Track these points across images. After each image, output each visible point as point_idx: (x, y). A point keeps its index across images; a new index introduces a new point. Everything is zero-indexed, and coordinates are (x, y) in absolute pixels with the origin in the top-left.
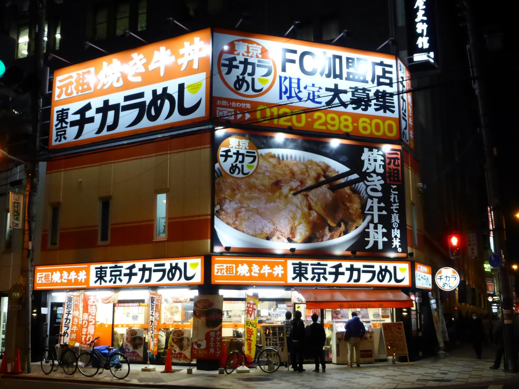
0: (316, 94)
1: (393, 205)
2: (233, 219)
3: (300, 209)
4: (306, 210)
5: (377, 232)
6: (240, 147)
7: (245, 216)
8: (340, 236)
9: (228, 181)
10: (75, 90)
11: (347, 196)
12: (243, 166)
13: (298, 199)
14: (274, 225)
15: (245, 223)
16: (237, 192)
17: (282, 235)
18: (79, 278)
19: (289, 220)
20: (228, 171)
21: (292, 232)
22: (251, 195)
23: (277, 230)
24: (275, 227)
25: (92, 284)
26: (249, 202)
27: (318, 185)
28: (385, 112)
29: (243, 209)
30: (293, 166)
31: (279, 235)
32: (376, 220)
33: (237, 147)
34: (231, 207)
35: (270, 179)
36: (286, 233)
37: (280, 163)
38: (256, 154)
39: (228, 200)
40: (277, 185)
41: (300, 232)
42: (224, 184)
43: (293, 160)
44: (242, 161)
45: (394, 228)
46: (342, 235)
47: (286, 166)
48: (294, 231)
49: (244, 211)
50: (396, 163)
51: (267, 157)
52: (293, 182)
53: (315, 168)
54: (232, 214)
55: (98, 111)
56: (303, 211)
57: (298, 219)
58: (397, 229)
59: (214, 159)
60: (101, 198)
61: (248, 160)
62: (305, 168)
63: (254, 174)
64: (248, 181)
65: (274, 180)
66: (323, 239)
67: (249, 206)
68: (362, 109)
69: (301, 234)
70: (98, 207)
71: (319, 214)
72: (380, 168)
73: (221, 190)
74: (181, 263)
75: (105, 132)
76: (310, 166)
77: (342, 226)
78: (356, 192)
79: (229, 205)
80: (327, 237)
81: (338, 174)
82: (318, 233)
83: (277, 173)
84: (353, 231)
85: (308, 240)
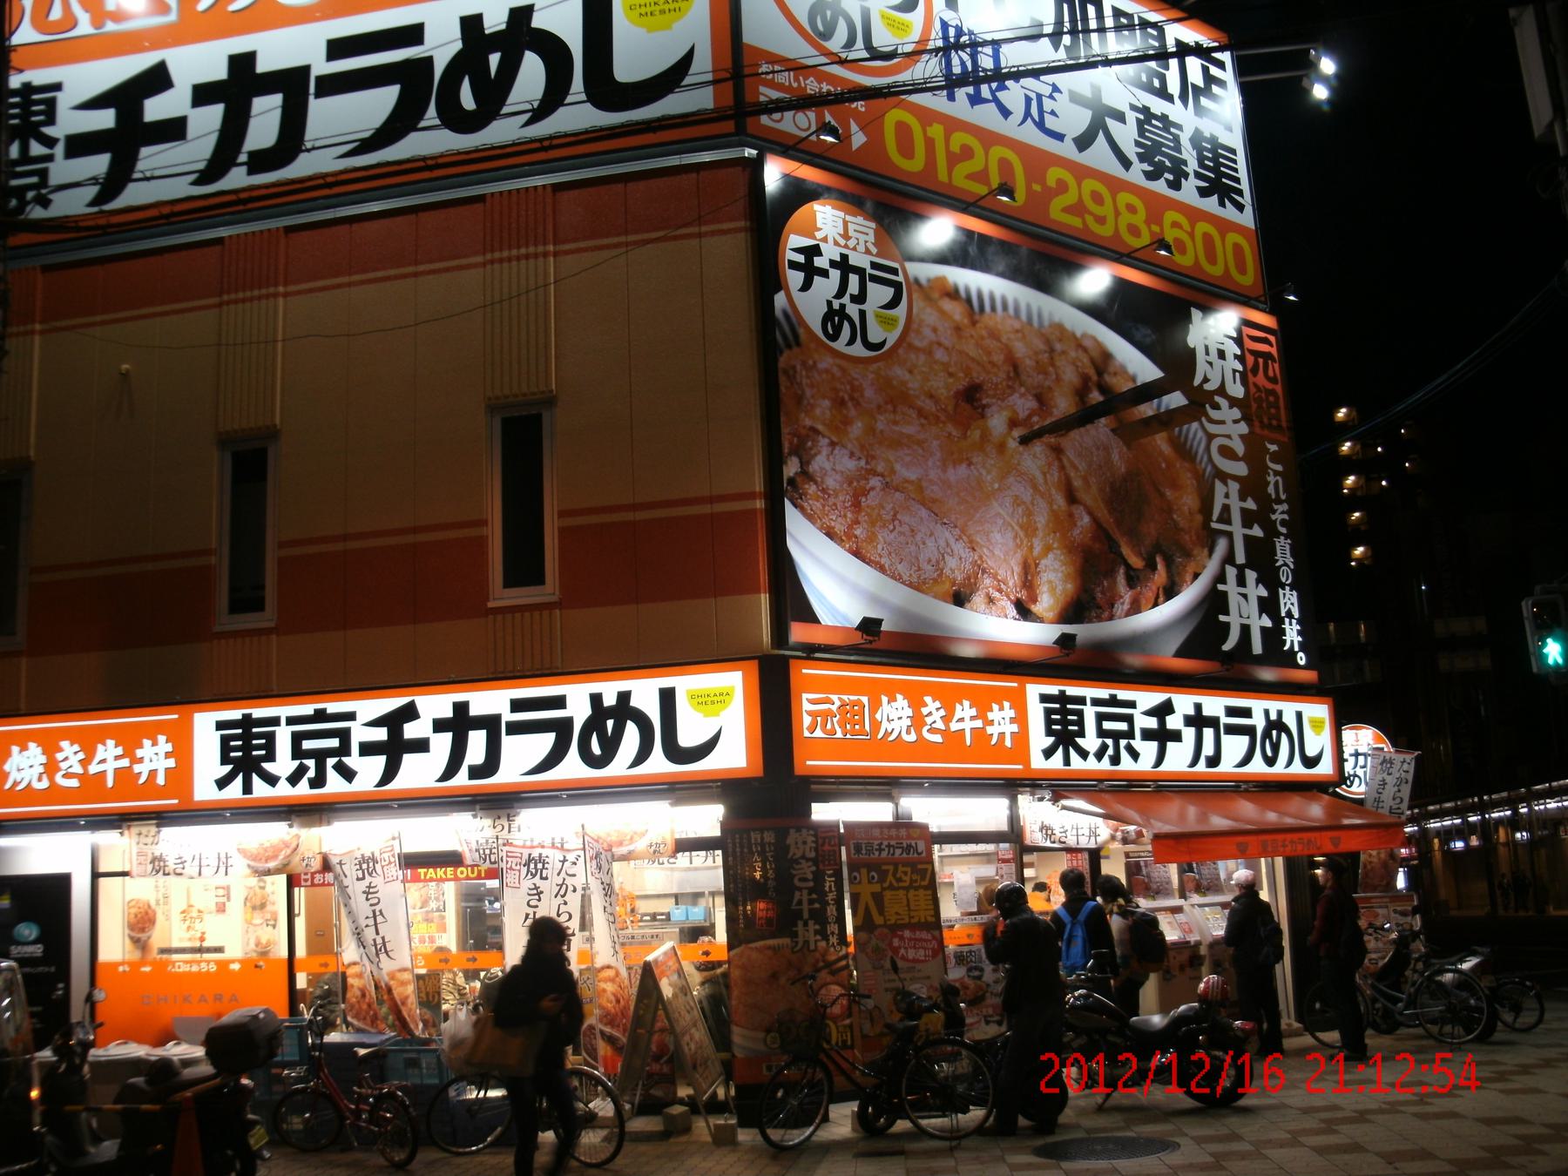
0: (1048, 105)
1: (1276, 507)
2: (845, 516)
3: (1042, 495)
4: (1060, 501)
5: (1245, 596)
6: (851, 243)
7: (883, 508)
8: (1156, 605)
9: (822, 366)
10: (87, 11)
11: (1164, 465)
12: (862, 314)
13: (1034, 459)
14: (974, 549)
15: (883, 536)
16: (853, 412)
17: (1000, 591)
18: (142, 769)
19: (1016, 537)
20: (815, 325)
21: (1026, 577)
22: (897, 428)
23: (984, 571)
24: (976, 558)
25: (204, 790)
26: (891, 455)
27: (1086, 416)
28: (1222, 204)
29: (875, 482)
30: (1012, 336)
31: (990, 589)
32: (1240, 558)
33: (842, 242)
34: (838, 467)
35: (951, 375)
36: (1011, 584)
37: (974, 323)
38: (900, 278)
39: (826, 441)
40: (971, 398)
41: (1050, 582)
42: (808, 377)
43: (1010, 317)
44: (860, 298)
45: (1283, 586)
46: (1161, 599)
47: (994, 335)
48: (1033, 577)
49: (878, 489)
50: (1271, 373)
51: (936, 295)
52: (1017, 395)
53: (1073, 354)
54: (841, 498)
55: (203, 94)
56: (1051, 506)
57: (1040, 534)
58: (1291, 590)
59: (767, 276)
60: (224, 441)
61: (879, 294)
62: (1046, 352)
63: (901, 351)
64: (883, 373)
65: (962, 384)
66: (1114, 610)
67: (893, 472)
68: (1167, 180)
69: (1052, 590)
70: (215, 473)
71: (1095, 520)
72: (1235, 382)
73: (799, 399)
74: (645, 693)
75: (237, 178)
76: (1058, 347)
77: (1159, 567)
78: (1184, 451)
79: (828, 459)
80: (1123, 604)
81: (1134, 386)
82: (1098, 589)
83: (967, 355)
84: (1188, 586)
85: (1074, 611)
